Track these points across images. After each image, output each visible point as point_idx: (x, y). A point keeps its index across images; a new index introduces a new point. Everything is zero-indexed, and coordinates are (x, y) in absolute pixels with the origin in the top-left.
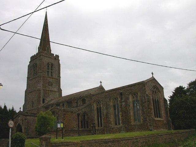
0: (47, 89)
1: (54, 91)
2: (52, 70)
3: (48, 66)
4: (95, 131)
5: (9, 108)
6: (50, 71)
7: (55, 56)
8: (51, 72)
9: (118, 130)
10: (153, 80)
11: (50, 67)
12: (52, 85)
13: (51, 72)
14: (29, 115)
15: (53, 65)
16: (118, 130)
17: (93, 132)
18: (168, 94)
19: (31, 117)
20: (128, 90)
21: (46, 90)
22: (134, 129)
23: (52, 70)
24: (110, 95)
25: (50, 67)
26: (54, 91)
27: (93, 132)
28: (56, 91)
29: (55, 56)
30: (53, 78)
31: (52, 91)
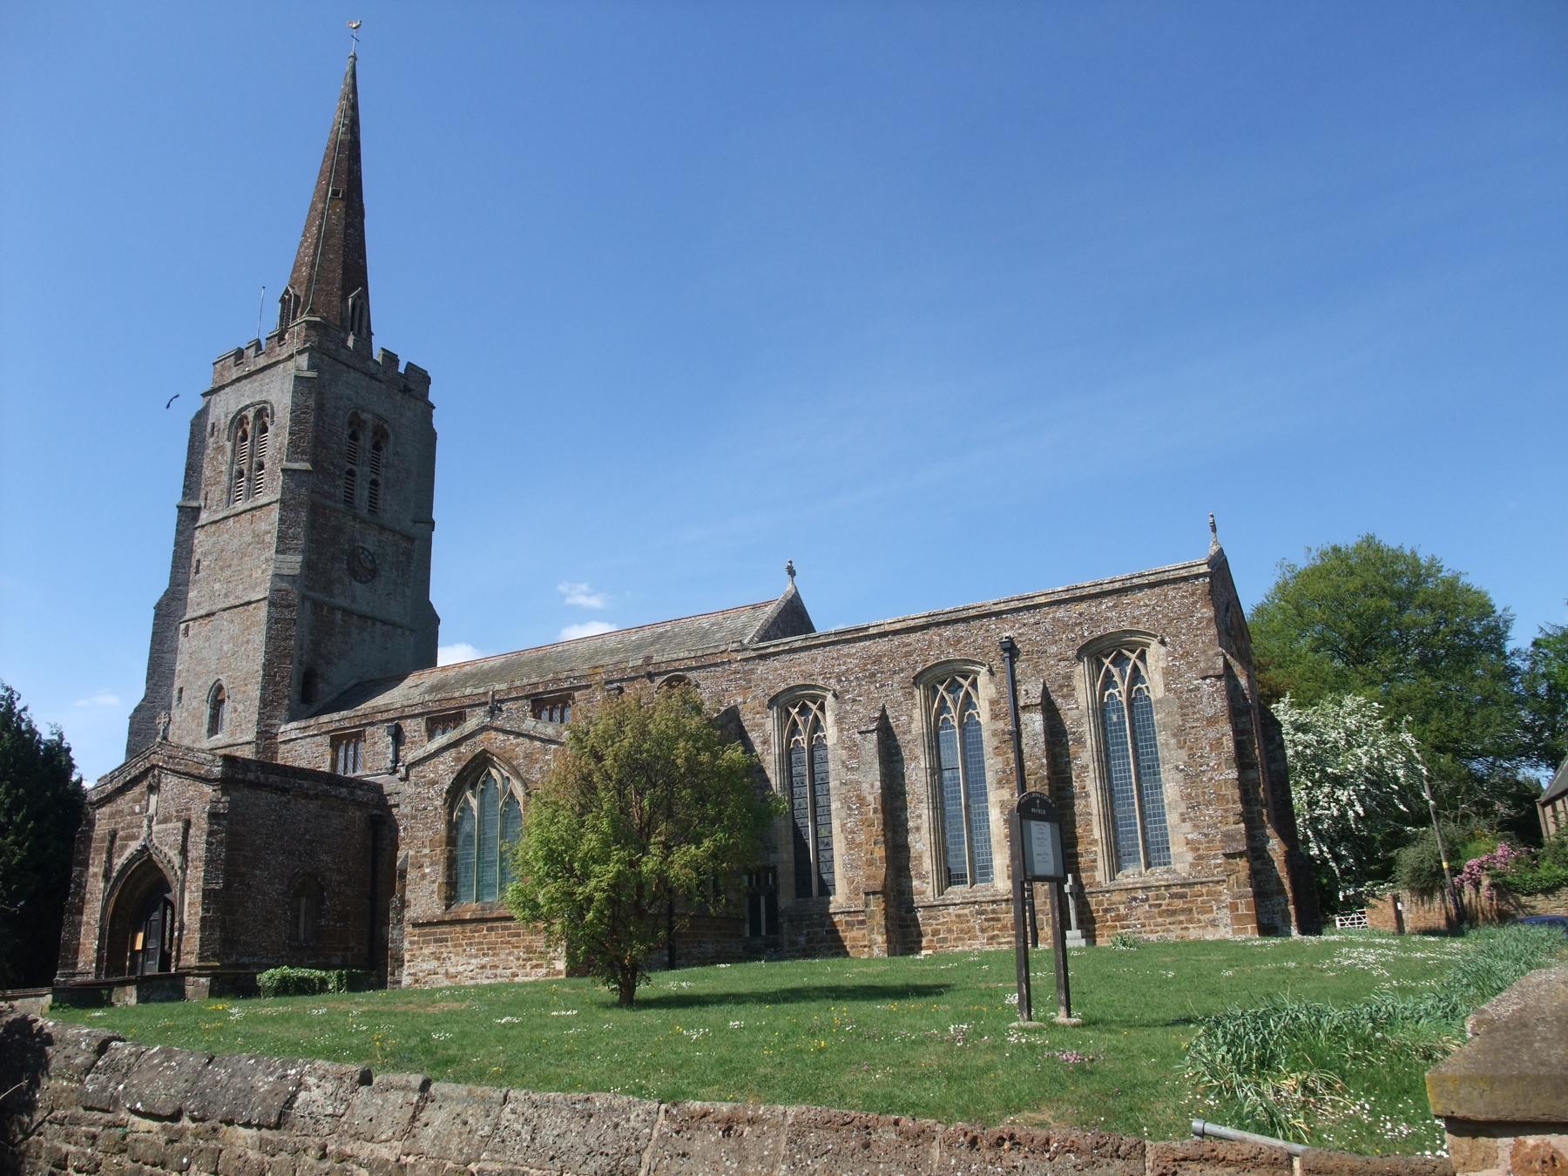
0: (340, 601)
1: (384, 623)
2: (375, 465)
3: (354, 437)
4: (774, 927)
5: (1424, 558)
6: (363, 472)
7: (401, 369)
8: (374, 483)
9: (976, 923)
10: (382, 984)
11: (366, 441)
12: (374, 573)
13: (374, 483)
14: (243, 781)
15: (385, 436)
16: (976, 923)
17: (755, 931)
18: (1209, 570)
19: (266, 797)
20: (1067, 627)
21: (333, 609)
22: (1119, 918)
23: (375, 465)
24: (908, 654)
25: (366, 441)
26: (384, 623)
27: (755, 931)
28: (395, 625)
29: (401, 369)
30: (383, 528)
31: (375, 619)
